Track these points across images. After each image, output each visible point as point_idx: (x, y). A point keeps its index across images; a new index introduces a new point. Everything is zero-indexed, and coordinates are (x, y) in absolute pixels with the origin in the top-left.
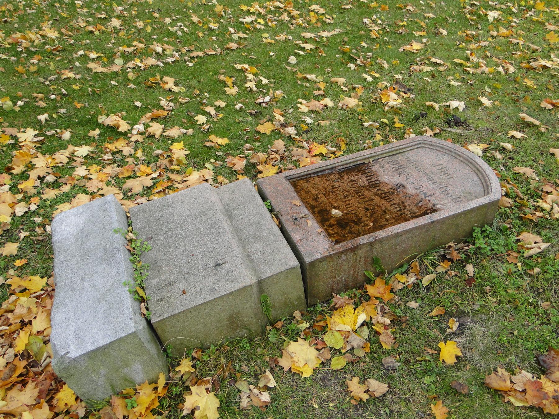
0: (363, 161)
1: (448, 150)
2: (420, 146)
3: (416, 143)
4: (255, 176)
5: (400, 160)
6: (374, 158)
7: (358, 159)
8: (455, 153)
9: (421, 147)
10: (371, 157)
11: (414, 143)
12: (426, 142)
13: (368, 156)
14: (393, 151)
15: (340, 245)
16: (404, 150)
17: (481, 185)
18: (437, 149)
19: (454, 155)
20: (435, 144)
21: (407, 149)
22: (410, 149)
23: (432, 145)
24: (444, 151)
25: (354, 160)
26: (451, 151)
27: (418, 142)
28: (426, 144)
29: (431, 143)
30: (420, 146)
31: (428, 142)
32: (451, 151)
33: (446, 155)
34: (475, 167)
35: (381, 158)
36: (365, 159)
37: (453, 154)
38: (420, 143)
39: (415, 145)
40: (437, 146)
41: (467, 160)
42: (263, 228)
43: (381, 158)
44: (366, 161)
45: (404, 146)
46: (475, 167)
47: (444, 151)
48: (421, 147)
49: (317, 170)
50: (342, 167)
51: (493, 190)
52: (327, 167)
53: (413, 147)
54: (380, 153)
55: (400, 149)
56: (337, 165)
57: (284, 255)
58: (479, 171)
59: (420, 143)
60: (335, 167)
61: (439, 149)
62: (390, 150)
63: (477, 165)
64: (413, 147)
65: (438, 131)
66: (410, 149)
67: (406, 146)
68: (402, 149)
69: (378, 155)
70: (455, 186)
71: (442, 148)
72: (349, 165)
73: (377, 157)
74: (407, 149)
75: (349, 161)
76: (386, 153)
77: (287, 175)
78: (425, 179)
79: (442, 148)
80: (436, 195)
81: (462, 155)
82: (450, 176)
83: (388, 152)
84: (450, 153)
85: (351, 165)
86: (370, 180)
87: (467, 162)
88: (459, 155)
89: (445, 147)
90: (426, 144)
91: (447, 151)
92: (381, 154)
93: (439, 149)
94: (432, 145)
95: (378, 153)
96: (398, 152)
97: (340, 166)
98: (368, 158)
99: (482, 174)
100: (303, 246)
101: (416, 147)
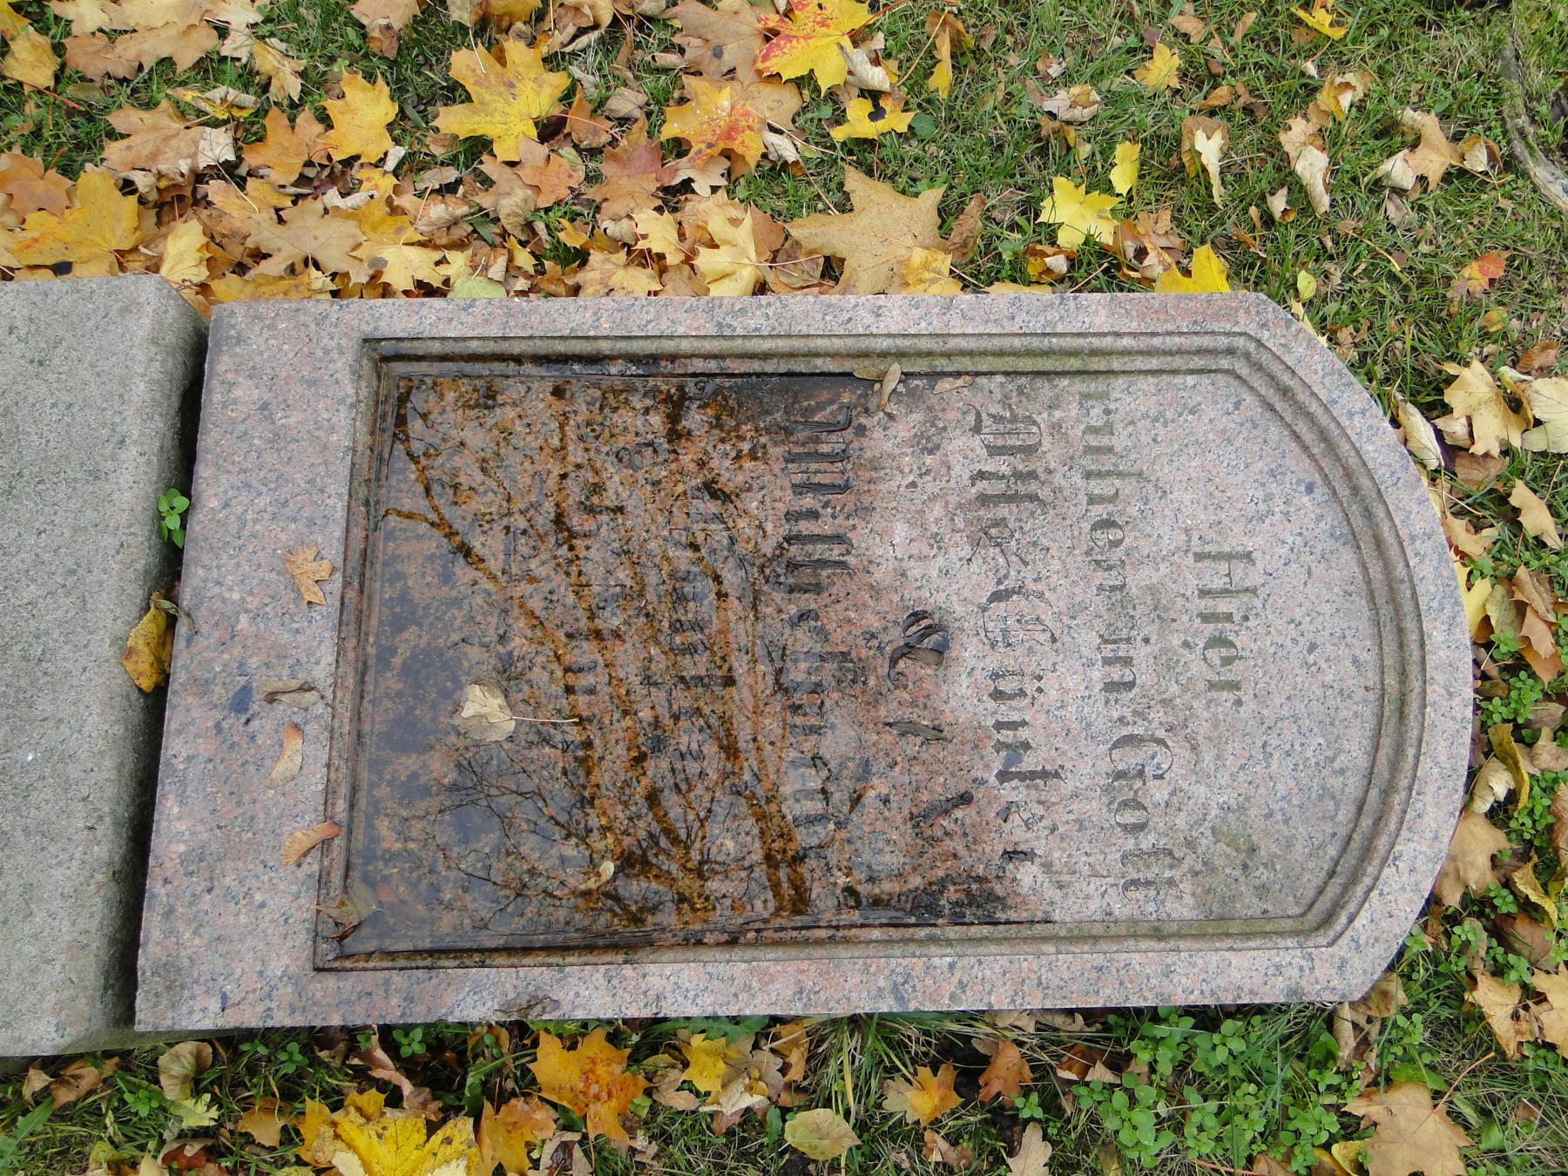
0: (847, 366)
1: (1348, 474)
2: (1225, 363)
3: (1207, 342)
4: (427, 102)
5: (1056, 427)
6: (921, 366)
7: (821, 344)
8: (1368, 514)
9: (1229, 372)
10: (900, 355)
11: (1198, 341)
12: (1265, 358)
13: (885, 344)
14: (1046, 353)
15: (350, 984)
16: (1116, 364)
17: (1345, 814)
18: (1302, 428)
19: (1358, 521)
20: (1303, 397)
21: (1140, 363)
22: (1154, 363)
23: (1285, 392)
24: (1326, 463)
25: (798, 344)
26: (1355, 490)
27: (1223, 342)
28: (1259, 368)
29: (1286, 379)
30: (1225, 363)
31: (1276, 369)
32: (1355, 490)
33: (1321, 493)
34: (1403, 675)
35: (958, 374)
36: (865, 355)
37: (1355, 509)
38: (1230, 352)
39: (1199, 352)
40: (1309, 417)
41: (1393, 599)
42: (44, 706)
43: (958, 374)
44: (861, 369)
45: (1126, 342)
46: (1403, 675)
47: (1326, 463)
48: (1229, 372)
49: (560, 347)
50: (712, 366)
51: (1362, 920)
52: (622, 346)
53: (1178, 362)
54: (963, 344)
55: (1094, 353)
56: (685, 346)
57: (30, 949)
58: (1402, 716)
59: (1230, 352)
60: (673, 358)
61: (1308, 437)
62: (1035, 343)
63: (1414, 670)
64: (1178, 362)
65: (1478, 161)
66: (1154, 363)
67: (1142, 343)
68: (1109, 353)
69: (948, 355)
70: (1208, 757)
71: (1324, 436)
72: (756, 366)
73: (942, 364)
74: (1140, 363)
75: (767, 345)
76: (1000, 353)
77: (385, 329)
78: (1087, 639)
79: (1324, 436)
80: (1068, 786)
81: (1393, 551)
82: (1235, 672)
83: (1016, 354)
84: (1344, 492)
85: (769, 367)
86: (806, 527)
87: (1386, 611)
88: (1379, 543)
89: (1345, 448)
90: (1259, 368)
91: (1336, 475)
92: (971, 354)
93: (1308, 437)
94: (1285, 392)
95: (952, 344)
96: (1075, 364)
97: (707, 357)
98: (884, 355)
99: (1399, 750)
100: (170, 912)
101: (1198, 362)
